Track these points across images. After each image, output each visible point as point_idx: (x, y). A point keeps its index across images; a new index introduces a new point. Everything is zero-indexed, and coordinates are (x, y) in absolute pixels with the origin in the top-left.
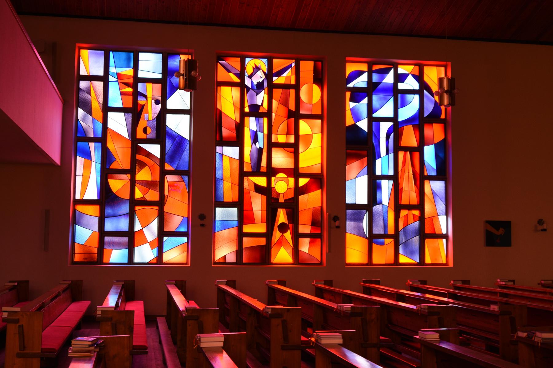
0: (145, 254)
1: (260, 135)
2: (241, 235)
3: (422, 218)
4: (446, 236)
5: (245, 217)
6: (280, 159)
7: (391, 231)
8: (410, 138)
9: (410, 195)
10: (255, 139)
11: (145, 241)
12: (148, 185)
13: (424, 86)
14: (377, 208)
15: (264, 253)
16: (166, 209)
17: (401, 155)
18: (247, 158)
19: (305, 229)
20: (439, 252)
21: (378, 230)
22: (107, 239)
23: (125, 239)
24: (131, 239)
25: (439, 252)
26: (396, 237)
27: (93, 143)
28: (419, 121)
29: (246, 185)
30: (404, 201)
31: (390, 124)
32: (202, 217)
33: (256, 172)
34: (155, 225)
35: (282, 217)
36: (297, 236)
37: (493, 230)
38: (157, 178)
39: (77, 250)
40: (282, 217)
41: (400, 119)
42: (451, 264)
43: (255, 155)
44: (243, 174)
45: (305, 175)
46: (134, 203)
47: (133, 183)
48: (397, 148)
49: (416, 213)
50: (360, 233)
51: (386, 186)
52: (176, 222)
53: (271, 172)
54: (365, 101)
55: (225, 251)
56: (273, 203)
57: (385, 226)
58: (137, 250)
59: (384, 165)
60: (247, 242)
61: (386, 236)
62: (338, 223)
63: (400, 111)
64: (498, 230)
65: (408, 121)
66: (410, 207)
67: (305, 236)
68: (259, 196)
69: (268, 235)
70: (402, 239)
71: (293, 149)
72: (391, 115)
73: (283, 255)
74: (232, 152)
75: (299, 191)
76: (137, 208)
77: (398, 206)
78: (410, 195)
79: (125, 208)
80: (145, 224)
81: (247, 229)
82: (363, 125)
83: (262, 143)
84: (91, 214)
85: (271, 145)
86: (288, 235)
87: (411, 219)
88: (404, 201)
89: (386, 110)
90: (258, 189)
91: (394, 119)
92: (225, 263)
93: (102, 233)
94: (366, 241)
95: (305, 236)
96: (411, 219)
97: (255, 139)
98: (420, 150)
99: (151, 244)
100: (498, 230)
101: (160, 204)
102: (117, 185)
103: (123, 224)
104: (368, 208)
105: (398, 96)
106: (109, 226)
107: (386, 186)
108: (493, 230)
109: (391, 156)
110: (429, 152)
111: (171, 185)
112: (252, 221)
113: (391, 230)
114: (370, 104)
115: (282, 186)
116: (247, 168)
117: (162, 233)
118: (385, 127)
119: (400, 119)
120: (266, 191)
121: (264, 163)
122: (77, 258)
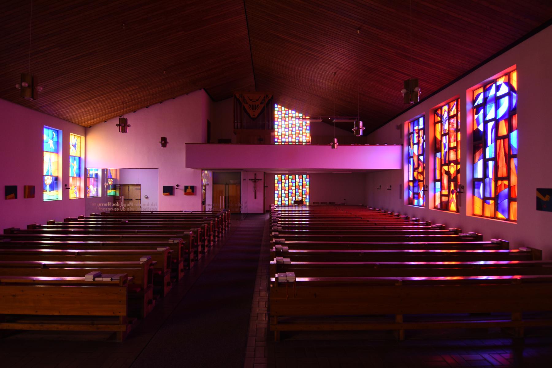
7: (493, 196)
8: (503, 131)
10: (445, 148)
14: (487, 180)
21: (488, 195)
23: (227, 186)
27: (45, 194)
30: (500, 175)
31: (493, 123)
37: (541, 197)
49: (506, 182)
50: (480, 197)
51: (491, 164)
59: (490, 152)
61: (490, 198)
64: (544, 196)
66: (503, 179)
72: (493, 117)
77: (497, 178)
78: (503, 171)
82: (481, 128)
87: (503, 187)
94: (482, 201)
96: (503, 187)
97: (445, 148)
98: (508, 137)
100: (544, 196)
105: (497, 100)
107: (491, 164)
108: (541, 197)
109: (493, 144)
110: (514, 135)
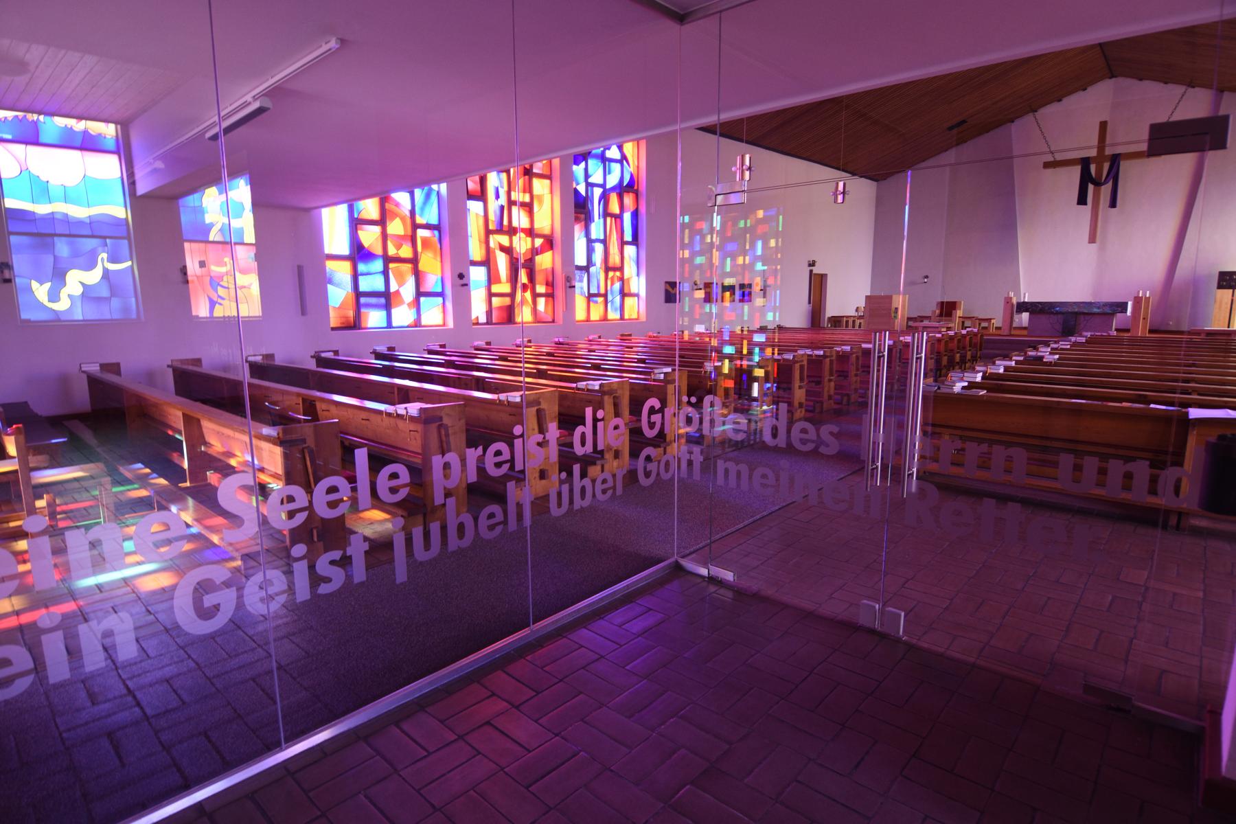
0: (402, 316)
1: (500, 190)
2: (491, 295)
3: (622, 279)
4: (637, 295)
5: (492, 278)
6: (520, 219)
9: (615, 259)
10: (497, 197)
11: (402, 302)
12: (399, 240)
13: (624, 157)
15: (509, 315)
16: (421, 266)
17: (609, 219)
18: (492, 217)
19: (541, 289)
20: (633, 308)
21: (594, 290)
22: (363, 300)
23: (383, 300)
24: (387, 299)
25: (633, 308)
26: (605, 296)
28: (621, 189)
29: (492, 245)
30: (611, 264)
32: (461, 276)
33: (500, 230)
34: (411, 282)
35: (523, 278)
36: (535, 296)
38: (409, 233)
39: (332, 314)
40: (523, 278)
41: (608, 186)
42: (451, 324)
43: (498, 212)
44: (488, 232)
45: (539, 236)
46: (388, 260)
47: (384, 236)
48: (606, 214)
50: (582, 294)
51: (599, 248)
52: (433, 282)
53: (512, 231)
54: (583, 164)
55: (478, 310)
56: (522, 265)
57: (599, 287)
58: (394, 311)
59: (597, 230)
60: (496, 301)
62: (464, 281)
63: (608, 177)
65: (613, 189)
66: (615, 269)
67: (540, 295)
68: (503, 255)
69: (512, 295)
70: (610, 298)
71: (528, 207)
72: (601, 181)
73: (525, 315)
74: (475, 207)
75: (535, 252)
76: (391, 265)
79: (378, 265)
80: (401, 283)
81: (496, 289)
83: (503, 200)
84: (341, 271)
85: (511, 203)
86: (528, 295)
88: (611, 264)
89: (597, 178)
90: (503, 249)
91: (603, 186)
92: (477, 324)
93: (358, 294)
95: (540, 295)
97: (497, 197)
99: (409, 305)
101: (414, 261)
102: (370, 236)
103: (377, 284)
104: (586, 269)
106: (365, 284)
107: (599, 248)
111: (425, 242)
112: (498, 281)
113: (602, 291)
114: (586, 170)
115: (522, 245)
116: (491, 227)
117: (419, 294)
118: (598, 192)
119: (608, 186)
120: (508, 250)
121: (505, 222)
122: (333, 324)
